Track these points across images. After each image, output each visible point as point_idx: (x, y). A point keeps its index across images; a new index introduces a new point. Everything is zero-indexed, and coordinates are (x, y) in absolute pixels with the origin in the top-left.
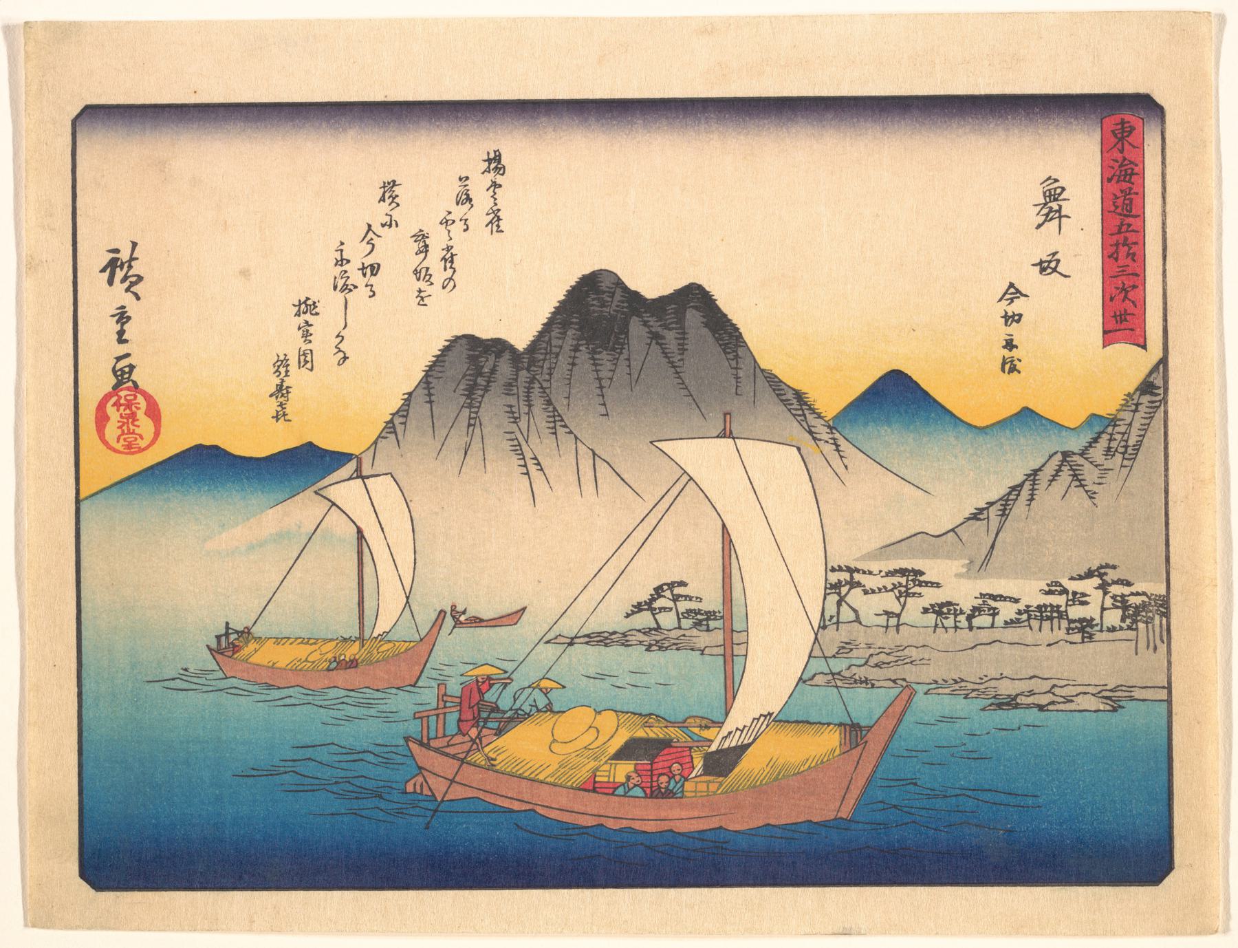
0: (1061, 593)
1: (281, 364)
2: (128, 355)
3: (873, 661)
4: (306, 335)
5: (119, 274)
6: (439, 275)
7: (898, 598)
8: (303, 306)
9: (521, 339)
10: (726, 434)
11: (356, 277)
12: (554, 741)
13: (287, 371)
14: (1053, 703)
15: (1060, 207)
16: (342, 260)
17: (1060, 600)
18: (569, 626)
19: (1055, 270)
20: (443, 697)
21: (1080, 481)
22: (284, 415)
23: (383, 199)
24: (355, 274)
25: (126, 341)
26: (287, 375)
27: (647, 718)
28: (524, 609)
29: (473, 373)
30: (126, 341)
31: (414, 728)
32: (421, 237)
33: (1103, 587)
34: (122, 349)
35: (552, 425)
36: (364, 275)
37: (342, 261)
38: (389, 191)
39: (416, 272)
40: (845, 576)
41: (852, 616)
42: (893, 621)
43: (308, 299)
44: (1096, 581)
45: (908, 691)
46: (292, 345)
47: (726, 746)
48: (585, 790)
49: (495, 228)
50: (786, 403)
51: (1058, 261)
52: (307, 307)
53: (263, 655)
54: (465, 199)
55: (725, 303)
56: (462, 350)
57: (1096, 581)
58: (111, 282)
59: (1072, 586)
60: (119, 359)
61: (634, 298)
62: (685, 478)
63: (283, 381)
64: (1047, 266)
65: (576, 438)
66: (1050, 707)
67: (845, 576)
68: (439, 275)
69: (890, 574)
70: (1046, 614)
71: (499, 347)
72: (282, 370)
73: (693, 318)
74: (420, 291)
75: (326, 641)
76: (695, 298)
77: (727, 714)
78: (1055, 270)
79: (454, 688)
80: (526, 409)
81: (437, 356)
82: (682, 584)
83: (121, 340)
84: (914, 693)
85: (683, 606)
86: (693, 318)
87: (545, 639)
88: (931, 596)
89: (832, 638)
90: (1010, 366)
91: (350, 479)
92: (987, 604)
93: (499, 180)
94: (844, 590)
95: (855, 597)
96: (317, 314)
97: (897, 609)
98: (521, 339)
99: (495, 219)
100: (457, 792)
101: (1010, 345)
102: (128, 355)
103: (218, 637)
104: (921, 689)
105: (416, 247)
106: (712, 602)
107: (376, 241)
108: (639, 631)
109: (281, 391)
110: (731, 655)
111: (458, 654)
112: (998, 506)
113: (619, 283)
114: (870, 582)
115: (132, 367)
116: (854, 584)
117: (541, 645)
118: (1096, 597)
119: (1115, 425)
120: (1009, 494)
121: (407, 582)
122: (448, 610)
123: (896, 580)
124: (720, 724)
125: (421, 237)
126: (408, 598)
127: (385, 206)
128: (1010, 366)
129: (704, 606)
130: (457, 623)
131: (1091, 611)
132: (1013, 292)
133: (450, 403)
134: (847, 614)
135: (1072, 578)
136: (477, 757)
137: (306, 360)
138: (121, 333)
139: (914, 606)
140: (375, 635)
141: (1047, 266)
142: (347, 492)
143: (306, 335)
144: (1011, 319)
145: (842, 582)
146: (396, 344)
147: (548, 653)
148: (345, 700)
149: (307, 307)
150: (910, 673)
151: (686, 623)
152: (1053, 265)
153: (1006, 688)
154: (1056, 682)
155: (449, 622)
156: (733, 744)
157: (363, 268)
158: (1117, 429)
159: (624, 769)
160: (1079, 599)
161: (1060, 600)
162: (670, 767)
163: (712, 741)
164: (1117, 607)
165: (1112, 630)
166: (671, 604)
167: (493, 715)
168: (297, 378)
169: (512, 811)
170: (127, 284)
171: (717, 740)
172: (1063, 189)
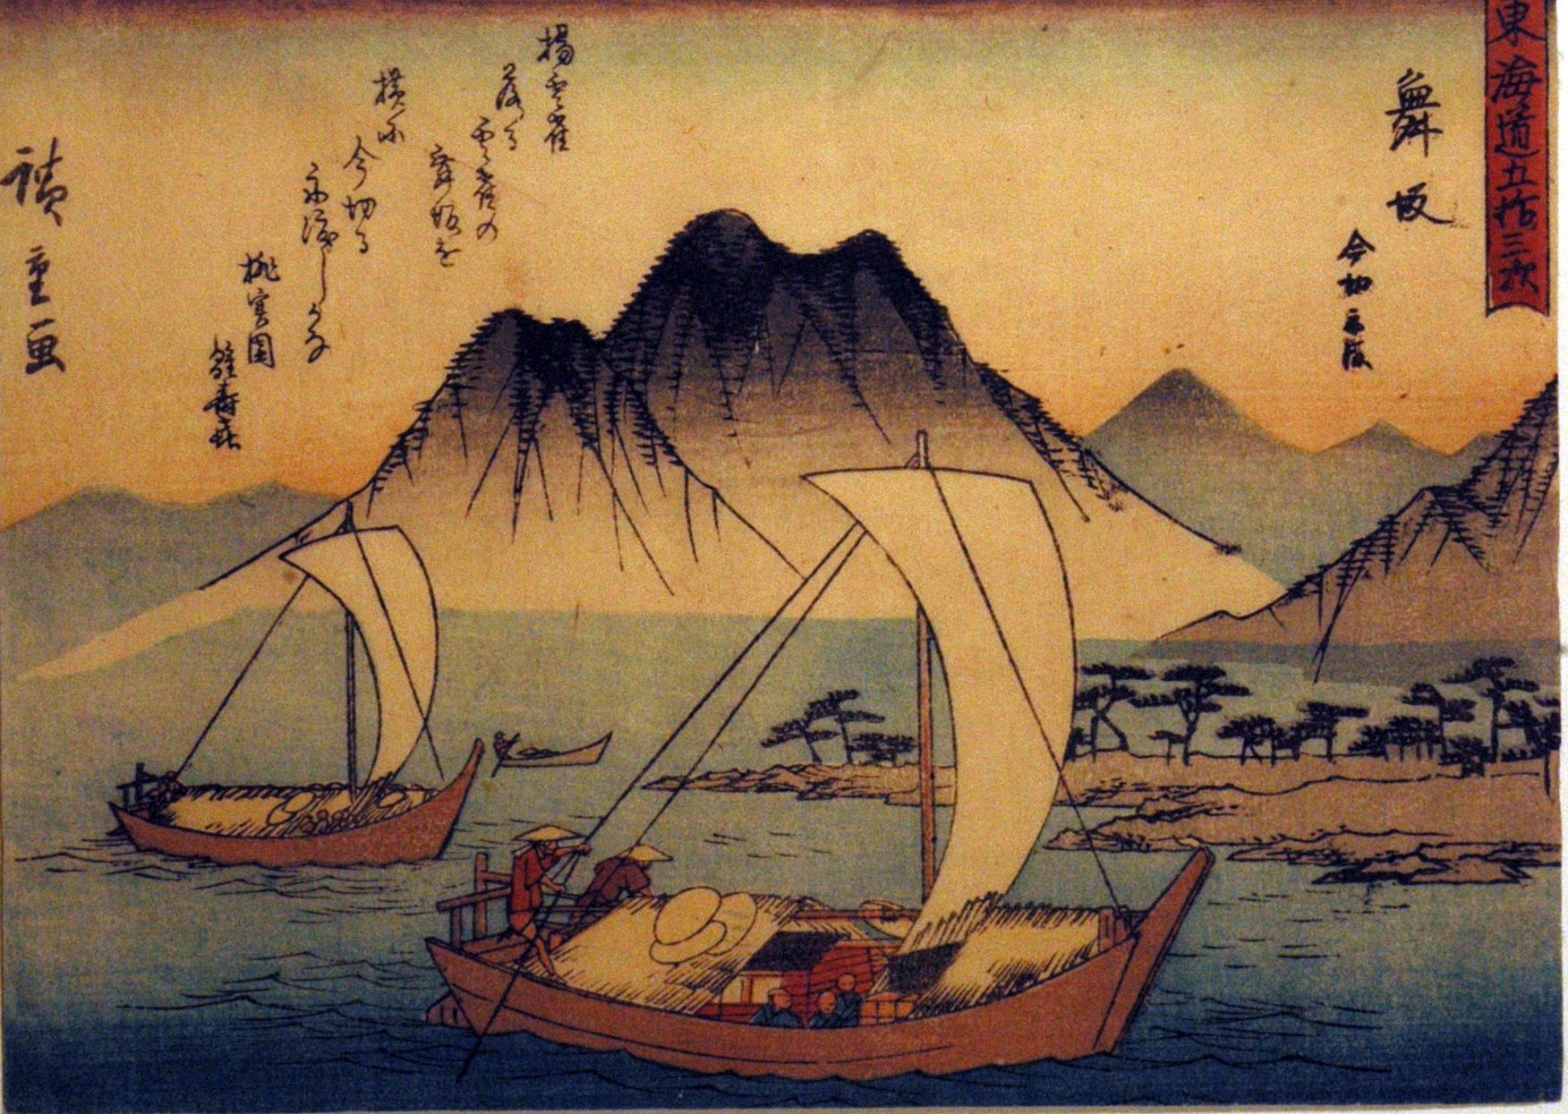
0: (1430, 702)
1: (222, 358)
2: (47, 321)
3: (1150, 809)
4: (260, 310)
5: (32, 188)
6: (472, 215)
7: (1186, 714)
8: (255, 266)
9: (599, 322)
10: (921, 463)
11: (338, 221)
12: (657, 941)
13: (231, 368)
14: (1419, 871)
15: (1426, 116)
16: (317, 192)
17: (1428, 713)
18: (678, 761)
19: (1419, 211)
20: (483, 876)
21: (1459, 531)
22: (231, 436)
23: (380, 98)
24: (326, 216)
25: (46, 299)
26: (232, 376)
27: (802, 906)
28: (609, 737)
29: (532, 371)
30: (46, 299)
31: (439, 926)
32: (441, 160)
33: (1496, 695)
34: (40, 312)
35: (649, 451)
36: (352, 216)
37: (315, 196)
38: (391, 86)
39: (436, 215)
40: (1103, 680)
41: (1115, 741)
42: (1178, 749)
43: (261, 254)
44: (1486, 683)
45: (1202, 860)
46: (238, 326)
47: (923, 945)
48: (707, 1017)
49: (558, 145)
50: (1011, 415)
51: (1424, 199)
52: (257, 267)
53: (194, 813)
54: (509, 97)
55: (914, 260)
56: (508, 336)
57: (1486, 683)
58: (21, 197)
59: (1450, 692)
60: (35, 326)
61: (774, 254)
62: (858, 531)
63: (225, 385)
64: (1408, 205)
65: (688, 471)
66: (1417, 878)
67: (1103, 680)
68: (472, 215)
69: (1169, 676)
70: (1403, 732)
71: (575, 330)
72: (223, 366)
73: (865, 280)
74: (441, 243)
75: (296, 790)
76: (871, 257)
77: (925, 899)
78: (1419, 211)
79: (501, 863)
80: (608, 426)
81: (469, 345)
82: (854, 694)
83: (37, 300)
84: (1210, 860)
85: (855, 728)
86: (865, 280)
87: (643, 782)
88: (1236, 708)
89: (1085, 774)
90: (1353, 357)
91: (336, 534)
92: (1322, 718)
93: (563, 73)
94: (1102, 703)
95: (1121, 713)
96: (277, 279)
97: (1181, 730)
98: (599, 322)
99: (558, 136)
100: (508, 1021)
101: (1353, 324)
102: (47, 321)
103: (123, 787)
104: (1221, 853)
105: (549, 128)
106: (898, 723)
107: (368, 163)
108: (789, 769)
109: (223, 404)
110: (931, 809)
111: (514, 804)
112: (1335, 571)
113: (753, 231)
114: (1141, 688)
115: (53, 340)
116: (1118, 694)
117: (635, 792)
118: (1483, 709)
119: (1512, 448)
120: (1352, 552)
121: (424, 698)
122: (489, 741)
123: (1183, 685)
124: (913, 916)
125: (441, 160)
126: (426, 720)
127: (385, 110)
128: (1353, 357)
129: (887, 729)
130: (503, 758)
131: (1479, 727)
132: (1356, 247)
133: (488, 419)
134: (1106, 739)
135: (1448, 681)
136: (538, 969)
137: (261, 353)
138: (36, 287)
139: (1209, 723)
140: (374, 778)
141: (1408, 205)
142: (333, 559)
143: (260, 310)
144: (1355, 285)
145: (1105, 685)
146: (400, 330)
147: (643, 804)
148: (327, 882)
149: (257, 267)
150: (1208, 827)
151: (861, 756)
152: (1417, 204)
153: (1359, 849)
154: (1425, 839)
155: (490, 758)
156: (935, 943)
157: (350, 206)
158: (1515, 454)
159: (766, 988)
160: (1460, 711)
161: (1428, 713)
162: (837, 981)
163: (903, 940)
164: (1519, 725)
165: (1510, 757)
166: (836, 727)
167: (561, 902)
168: (248, 382)
169: (590, 1051)
170: (45, 203)
171: (912, 937)
172: (1429, 90)
